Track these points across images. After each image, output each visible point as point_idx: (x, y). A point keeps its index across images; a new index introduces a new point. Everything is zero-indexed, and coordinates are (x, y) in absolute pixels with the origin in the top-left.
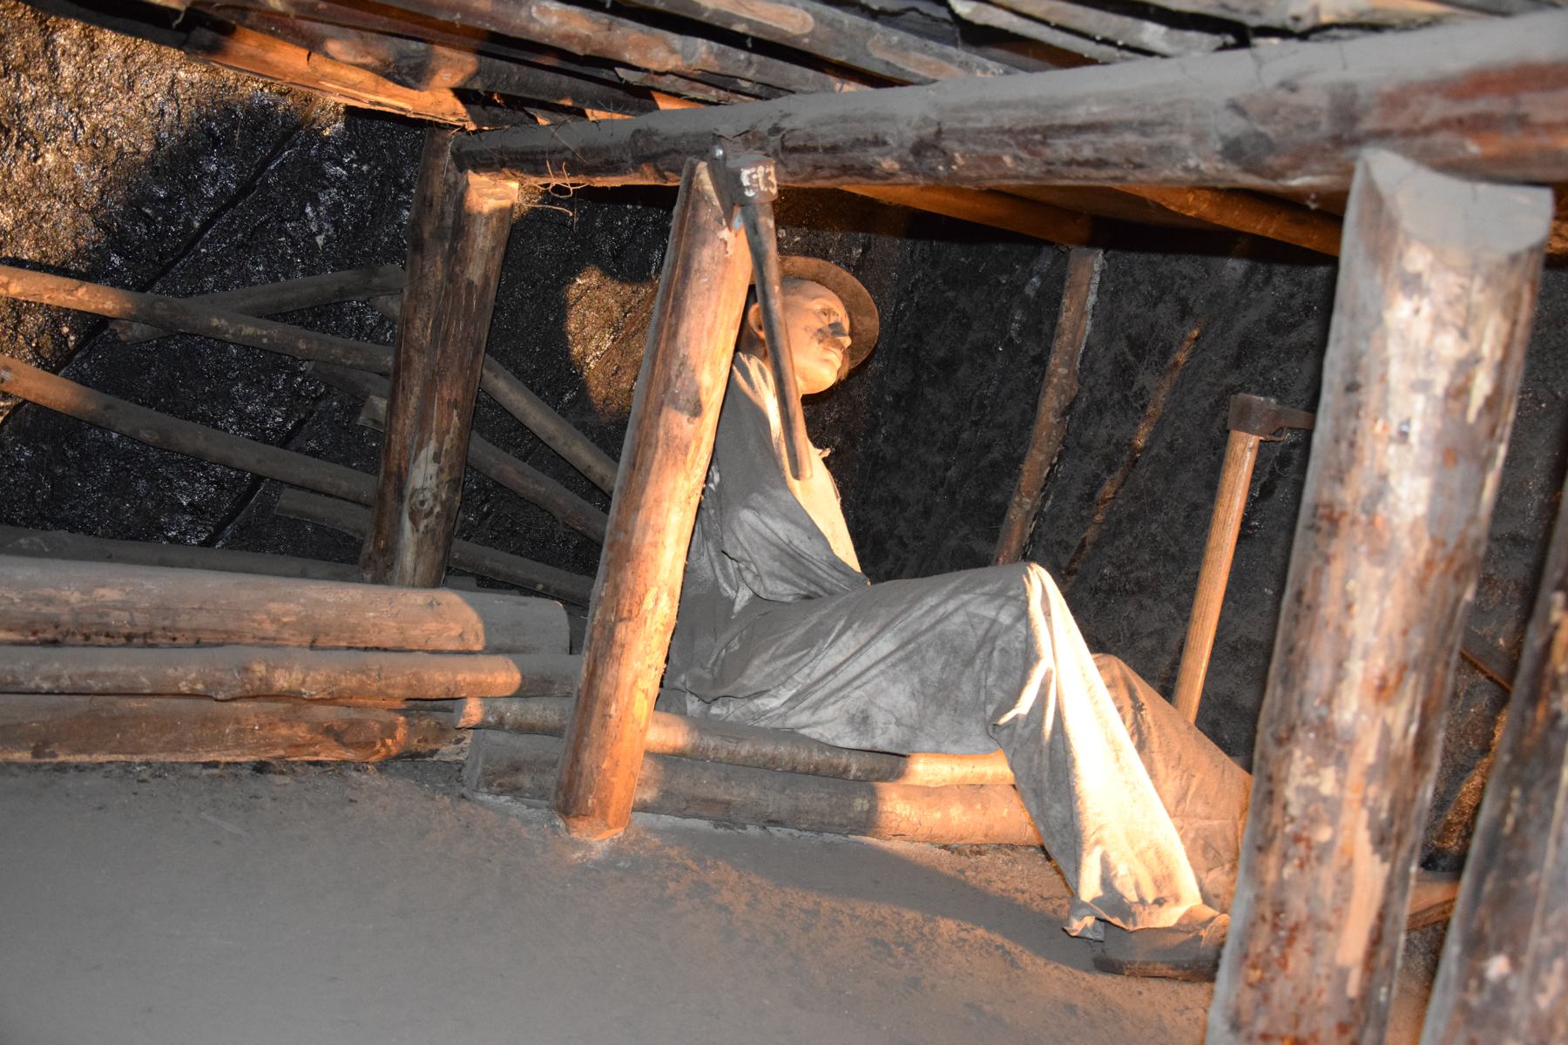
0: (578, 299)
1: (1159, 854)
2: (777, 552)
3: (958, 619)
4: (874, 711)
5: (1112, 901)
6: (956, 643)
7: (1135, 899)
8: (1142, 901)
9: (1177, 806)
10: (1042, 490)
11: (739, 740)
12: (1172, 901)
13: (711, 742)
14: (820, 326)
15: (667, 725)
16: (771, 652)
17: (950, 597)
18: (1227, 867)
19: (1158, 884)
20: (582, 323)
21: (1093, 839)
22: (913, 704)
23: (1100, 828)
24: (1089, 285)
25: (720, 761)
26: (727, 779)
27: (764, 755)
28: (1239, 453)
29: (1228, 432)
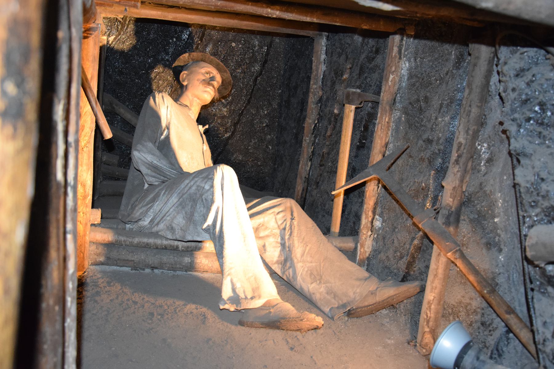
0: (155, 77)
1: (256, 279)
2: (148, 166)
3: (194, 188)
4: (174, 225)
5: (235, 299)
6: (194, 197)
7: (244, 297)
8: (246, 298)
9: (301, 258)
10: (313, 134)
11: (133, 238)
12: (257, 298)
13: (122, 238)
14: (204, 78)
15: (105, 233)
16: (141, 204)
17: (192, 180)
18: (318, 282)
19: (254, 290)
20: (158, 86)
21: (227, 274)
22: (184, 222)
23: (231, 269)
24: (321, 51)
25: (128, 246)
26: (132, 252)
27: (144, 243)
28: (347, 113)
29: (344, 105)
